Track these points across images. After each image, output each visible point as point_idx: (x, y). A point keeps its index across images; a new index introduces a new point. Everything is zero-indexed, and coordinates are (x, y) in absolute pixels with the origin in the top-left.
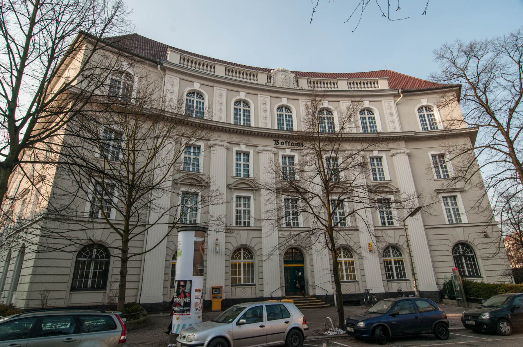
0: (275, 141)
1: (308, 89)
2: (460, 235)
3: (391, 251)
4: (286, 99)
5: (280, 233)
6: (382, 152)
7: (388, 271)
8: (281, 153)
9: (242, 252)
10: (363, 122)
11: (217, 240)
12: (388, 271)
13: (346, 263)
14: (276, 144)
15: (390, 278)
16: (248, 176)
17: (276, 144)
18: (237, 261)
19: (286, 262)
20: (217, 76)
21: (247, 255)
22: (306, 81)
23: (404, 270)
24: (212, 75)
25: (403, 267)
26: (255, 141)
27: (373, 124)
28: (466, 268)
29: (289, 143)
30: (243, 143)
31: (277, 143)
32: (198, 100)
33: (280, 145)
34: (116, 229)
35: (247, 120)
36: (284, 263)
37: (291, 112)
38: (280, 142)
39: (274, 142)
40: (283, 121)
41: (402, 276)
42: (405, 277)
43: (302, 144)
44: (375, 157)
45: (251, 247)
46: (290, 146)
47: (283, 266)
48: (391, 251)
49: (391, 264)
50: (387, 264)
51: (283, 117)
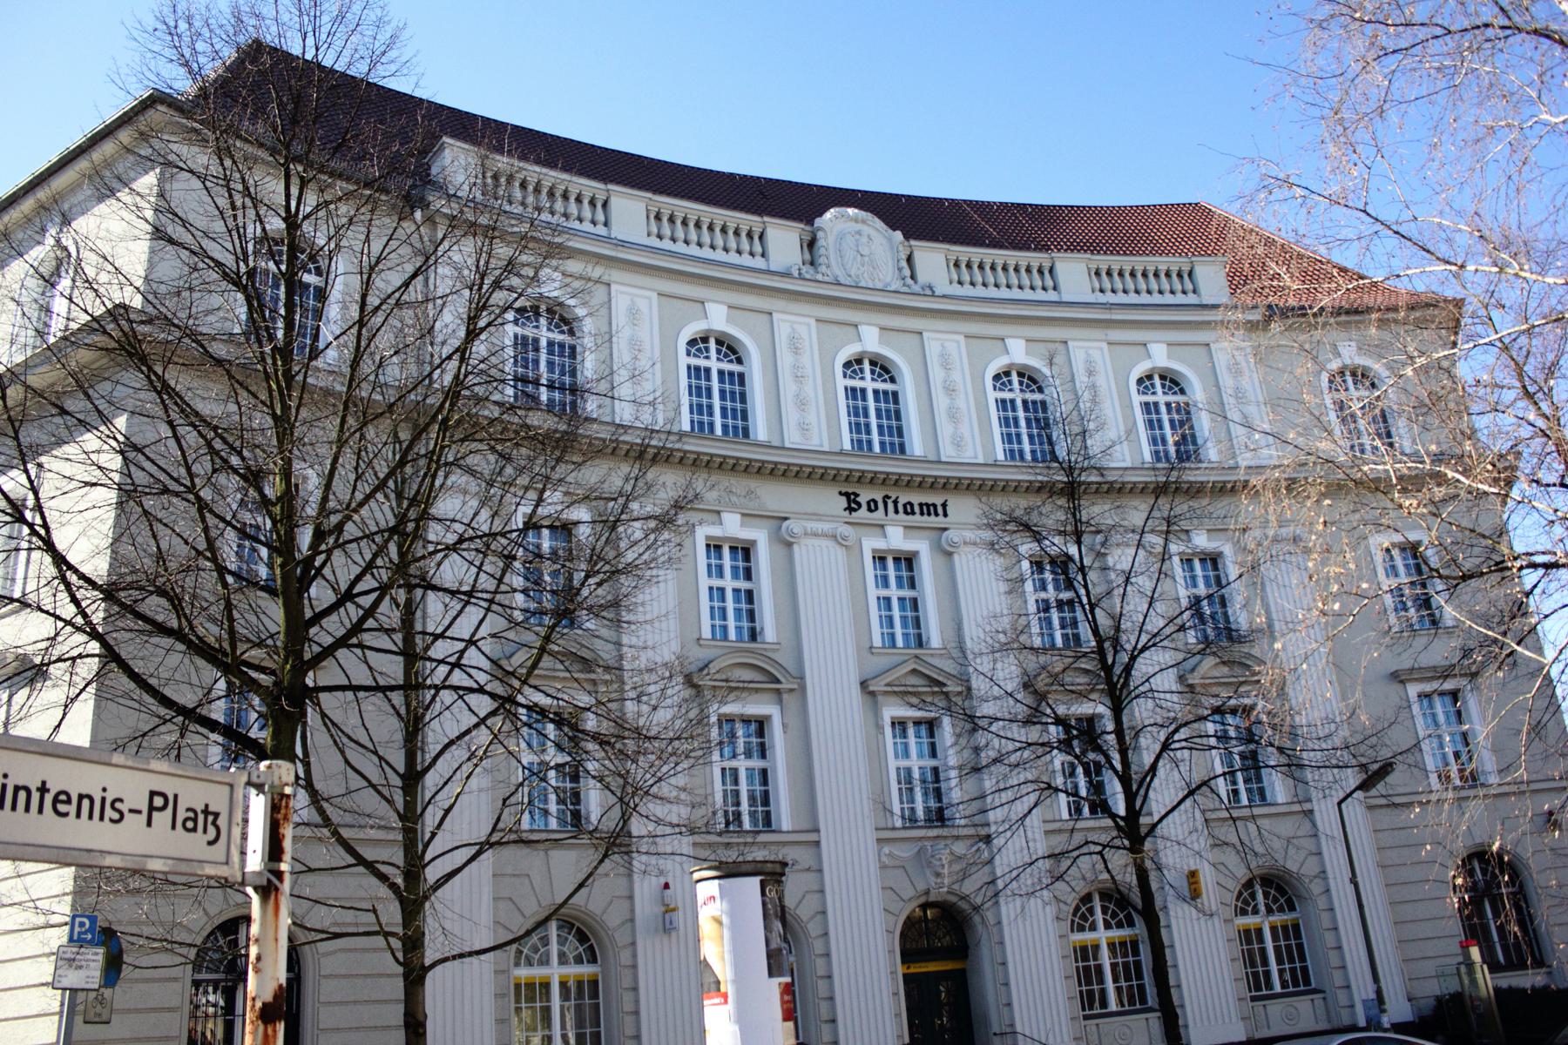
0: (847, 495)
1: (1091, 298)
2: (1477, 824)
3: (1098, 910)
4: (876, 330)
5: (886, 850)
6: (757, 521)
7: (1089, 983)
8: (871, 543)
9: (1257, 887)
10: (856, 408)
11: (667, 886)
12: (1089, 983)
13: (1111, 946)
14: (850, 509)
15: (1258, 988)
16: (753, 635)
17: (850, 509)
18: (1087, 936)
19: (907, 956)
20: (623, 244)
21: (1276, 900)
22: (1083, 267)
23: (1302, 958)
24: (607, 239)
25: (1300, 947)
26: (775, 496)
27: (700, 406)
28: (1496, 938)
29: (895, 503)
30: (733, 508)
31: (852, 504)
32: (551, 335)
33: (863, 512)
34: (370, 866)
35: (1038, 420)
36: (903, 962)
37: (893, 380)
38: (863, 499)
39: (843, 502)
40: (878, 411)
41: (1300, 981)
42: (1307, 982)
43: (944, 505)
44: (889, 551)
45: (1289, 872)
46: (901, 515)
47: (900, 970)
48: (1098, 910)
49: (1261, 940)
50: (1249, 942)
51: (864, 399)
